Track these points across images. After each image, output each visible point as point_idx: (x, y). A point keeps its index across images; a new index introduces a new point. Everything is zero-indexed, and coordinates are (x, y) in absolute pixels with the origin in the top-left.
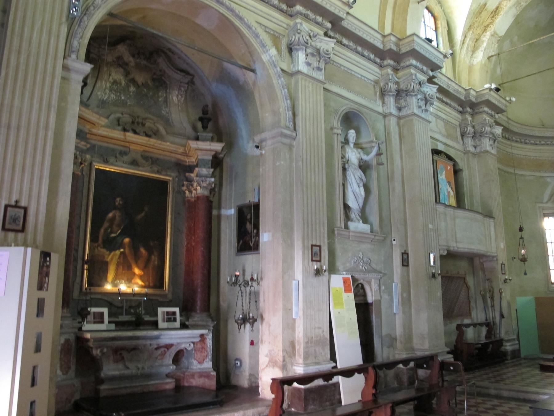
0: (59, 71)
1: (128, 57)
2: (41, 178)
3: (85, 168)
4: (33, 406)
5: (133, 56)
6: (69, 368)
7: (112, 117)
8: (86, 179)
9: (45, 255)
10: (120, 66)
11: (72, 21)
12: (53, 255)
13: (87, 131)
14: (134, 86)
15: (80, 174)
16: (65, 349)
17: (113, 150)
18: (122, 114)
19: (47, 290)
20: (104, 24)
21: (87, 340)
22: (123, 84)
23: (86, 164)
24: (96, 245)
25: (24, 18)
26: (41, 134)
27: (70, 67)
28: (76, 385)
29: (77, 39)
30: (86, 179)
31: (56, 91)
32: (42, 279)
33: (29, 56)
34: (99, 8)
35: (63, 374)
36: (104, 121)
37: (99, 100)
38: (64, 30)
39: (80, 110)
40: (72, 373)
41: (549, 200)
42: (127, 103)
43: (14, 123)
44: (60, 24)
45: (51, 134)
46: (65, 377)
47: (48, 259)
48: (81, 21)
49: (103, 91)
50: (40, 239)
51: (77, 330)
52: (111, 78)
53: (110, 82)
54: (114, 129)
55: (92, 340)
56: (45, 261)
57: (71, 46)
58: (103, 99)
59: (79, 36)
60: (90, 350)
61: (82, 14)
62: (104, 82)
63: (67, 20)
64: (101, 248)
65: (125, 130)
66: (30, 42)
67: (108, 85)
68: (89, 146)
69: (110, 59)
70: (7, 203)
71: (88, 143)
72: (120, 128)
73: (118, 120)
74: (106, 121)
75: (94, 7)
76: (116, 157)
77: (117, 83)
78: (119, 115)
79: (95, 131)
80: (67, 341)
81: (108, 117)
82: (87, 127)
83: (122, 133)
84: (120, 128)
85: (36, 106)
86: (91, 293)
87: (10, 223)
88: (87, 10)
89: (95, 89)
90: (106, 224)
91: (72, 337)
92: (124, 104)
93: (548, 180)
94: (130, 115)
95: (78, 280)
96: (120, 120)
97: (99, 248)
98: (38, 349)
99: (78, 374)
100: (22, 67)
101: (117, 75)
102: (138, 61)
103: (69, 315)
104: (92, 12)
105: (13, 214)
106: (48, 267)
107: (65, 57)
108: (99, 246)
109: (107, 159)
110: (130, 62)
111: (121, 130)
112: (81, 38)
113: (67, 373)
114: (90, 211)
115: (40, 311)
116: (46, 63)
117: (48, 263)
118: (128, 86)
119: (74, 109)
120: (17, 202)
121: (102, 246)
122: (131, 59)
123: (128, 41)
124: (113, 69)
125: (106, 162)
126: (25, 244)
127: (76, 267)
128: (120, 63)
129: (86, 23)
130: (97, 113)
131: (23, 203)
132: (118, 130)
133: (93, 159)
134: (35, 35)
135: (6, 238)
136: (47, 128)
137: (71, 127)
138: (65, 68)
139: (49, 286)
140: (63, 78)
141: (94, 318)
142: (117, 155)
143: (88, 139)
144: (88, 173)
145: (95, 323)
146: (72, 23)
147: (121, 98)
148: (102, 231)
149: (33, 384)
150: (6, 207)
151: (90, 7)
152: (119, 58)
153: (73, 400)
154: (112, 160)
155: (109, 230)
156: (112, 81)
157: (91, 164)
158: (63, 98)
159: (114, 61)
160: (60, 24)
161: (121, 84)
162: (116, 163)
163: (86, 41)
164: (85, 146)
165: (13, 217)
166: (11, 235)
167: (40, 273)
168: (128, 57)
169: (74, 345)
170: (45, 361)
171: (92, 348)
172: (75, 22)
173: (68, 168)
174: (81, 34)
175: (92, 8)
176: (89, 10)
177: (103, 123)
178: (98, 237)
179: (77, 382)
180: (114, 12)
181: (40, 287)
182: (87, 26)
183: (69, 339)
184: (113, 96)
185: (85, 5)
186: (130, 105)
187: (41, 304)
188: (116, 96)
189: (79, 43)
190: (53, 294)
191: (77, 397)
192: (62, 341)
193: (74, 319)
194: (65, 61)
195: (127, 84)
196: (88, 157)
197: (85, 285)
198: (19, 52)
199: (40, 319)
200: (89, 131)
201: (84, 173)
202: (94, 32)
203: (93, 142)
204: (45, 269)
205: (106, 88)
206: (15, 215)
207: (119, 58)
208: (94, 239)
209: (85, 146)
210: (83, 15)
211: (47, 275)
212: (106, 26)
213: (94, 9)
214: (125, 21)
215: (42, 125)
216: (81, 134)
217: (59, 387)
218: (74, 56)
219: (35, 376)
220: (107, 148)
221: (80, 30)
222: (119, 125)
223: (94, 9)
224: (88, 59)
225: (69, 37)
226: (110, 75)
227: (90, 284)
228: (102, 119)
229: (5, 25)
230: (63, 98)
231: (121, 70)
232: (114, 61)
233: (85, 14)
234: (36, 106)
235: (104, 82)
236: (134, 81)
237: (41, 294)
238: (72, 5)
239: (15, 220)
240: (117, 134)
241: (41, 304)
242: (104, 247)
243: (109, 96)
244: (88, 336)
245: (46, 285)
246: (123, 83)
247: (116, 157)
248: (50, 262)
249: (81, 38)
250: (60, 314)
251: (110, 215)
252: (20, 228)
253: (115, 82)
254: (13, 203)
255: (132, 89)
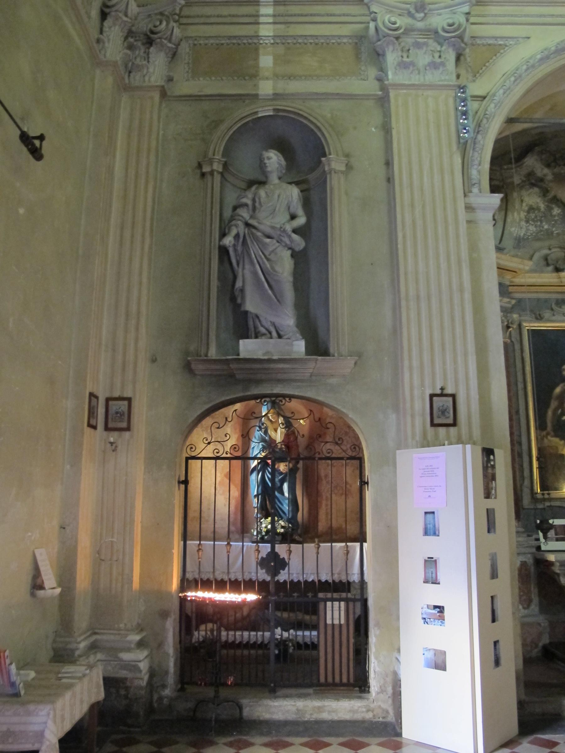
0: (462, 215)
1: (541, 171)
2: (466, 354)
3: (513, 333)
4: (497, 647)
5: (548, 166)
6: (530, 601)
7: (537, 256)
8: (517, 347)
9: (488, 452)
10: (533, 185)
11: (464, 147)
12: (496, 451)
13: (508, 283)
14: (559, 207)
15: (509, 341)
16: (523, 575)
17: (546, 301)
18: (550, 249)
19: (495, 498)
20: (500, 137)
21: (551, 564)
22: (542, 209)
23: (515, 327)
24: (544, 433)
25: (410, 162)
26: (456, 301)
27: (473, 205)
28: (542, 624)
29: (475, 167)
30: (517, 347)
31: (463, 240)
32: (488, 484)
33: (424, 207)
34: (493, 117)
35: (524, 608)
36: (528, 265)
37: (516, 239)
38: (458, 160)
39: (497, 258)
40: (535, 607)
42: (552, 233)
43: (423, 294)
44: (451, 157)
45: (467, 296)
46: (526, 611)
47: (492, 457)
48: (475, 143)
49: (519, 225)
50: (477, 433)
51: (534, 550)
52: (524, 204)
53: (524, 211)
54: (542, 272)
55: (558, 564)
56: (489, 460)
57: (469, 179)
58: (520, 236)
59: (476, 162)
60: (556, 577)
61: (474, 132)
62: (516, 214)
63: (458, 148)
64: (552, 437)
65: (557, 270)
66: (422, 190)
67: (523, 215)
68: (513, 302)
69: (517, 180)
70: (431, 392)
71: (513, 298)
72: (551, 268)
73: (546, 258)
74: (531, 263)
75: (487, 118)
76: (552, 309)
77: (533, 209)
78: (546, 251)
79: (518, 280)
80: (524, 564)
81: (531, 258)
82: (508, 278)
83: (555, 274)
84: (551, 268)
85: (444, 266)
86: (550, 500)
87: (439, 417)
88: (479, 126)
89: (507, 225)
90: (554, 404)
91: (529, 560)
92: (549, 234)
94: (560, 247)
95: (527, 482)
96: (549, 258)
97: (549, 437)
98: (494, 575)
99: (543, 609)
100: (419, 223)
101: (532, 198)
102: (556, 170)
103: (523, 530)
104: (487, 126)
105: (441, 404)
106: (493, 467)
107: (465, 196)
108: (548, 434)
109: (540, 315)
110: (545, 175)
111: (553, 272)
112: (480, 164)
113: (528, 607)
114: (529, 388)
115: (491, 527)
116: (445, 209)
117: (492, 463)
118: (550, 209)
119: (490, 258)
120: (442, 389)
121: (552, 433)
122: (546, 171)
123: (537, 149)
124: (524, 193)
125: (539, 318)
126: (459, 441)
127: (522, 466)
128: (533, 181)
129: (482, 142)
130: (516, 256)
131: (449, 391)
132: (548, 272)
133: (522, 318)
134: (425, 179)
135: (436, 435)
136: (461, 290)
137: (491, 282)
138: (469, 208)
139: (497, 491)
140: (469, 222)
141: (556, 534)
142: (554, 306)
143: (511, 293)
144: (518, 338)
145: (557, 540)
146: (465, 150)
147: (543, 227)
148: (550, 413)
149: (494, 620)
150: (432, 396)
151: (481, 121)
152: (531, 174)
153: (541, 644)
154: (547, 314)
155: (560, 411)
156: (526, 208)
157: (520, 326)
158: (473, 247)
159: (523, 181)
160: (451, 157)
161: (538, 209)
162: (554, 318)
163: (486, 166)
164: (509, 303)
165: (441, 408)
166: (442, 431)
167: (485, 476)
168: (541, 171)
169: (532, 569)
170: (506, 588)
171: (558, 575)
172: (468, 145)
173: (496, 339)
174: (479, 159)
175: (485, 121)
176: (482, 125)
177: (527, 268)
178: (546, 423)
179: (542, 619)
180: (513, 116)
181: (488, 495)
182: (483, 146)
183: (525, 562)
184: (532, 228)
185: (475, 121)
186: (558, 234)
187: (490, 514)
188: (536, 226)
189: (479, 172)
190: (503, 503)
191: (545, 640)
192: (518, 564)
193: (529, 536)
194: (467, 200)
195: (548, 206)
196: (515, 316)
197: (538, 489)
198: (412, 206)
199: (492, 535)
200: (512, 282)
201: (513, 339)
202: (494, 150)
203: (518, 296)
204: (490, 471)
205: (521, 220)
206: (443, 406)
207: (531, 174)
208: (541, 426)
209: (509, 303)
210: (476, 134)
211: (493, 478)
212: (507, 137)
213: (488, 121)
214: (531, 122)
215: (455, 287)
216: (504, 290)
217: (524, 625)
218: (475, 190)
219: (495, 608)
220: (538, 300)
221: (476, 154)
222: (548, 265)
223: (488, 121)
224: (494, 189)
225: (465, 167)
226: (522, 201)
227: (544, 487)
228: (526, 262)
229: (391, 179)
230: (473, 247)
231: (536, 190)
232: (523, 181)
233: (478, 132)
234: (444, 266)
235: (516, 214)
236: (558, 200)
237: (490, 503)
238: (460, 127)
239: (443, 412)
240: (548, 277)
241: (490, 514)
242: (556, 436)
243: (528, 230)
244: (551, 558)
245: (493, 492)
246: (542, 206)
247: (552, 309)
248: (494, 460)
249: (480, 164)
250: (514, 530)
251: (558, 390)
252: (451, 421)
253: (531, 209)
254: (439, 392)
255: (556, 211)
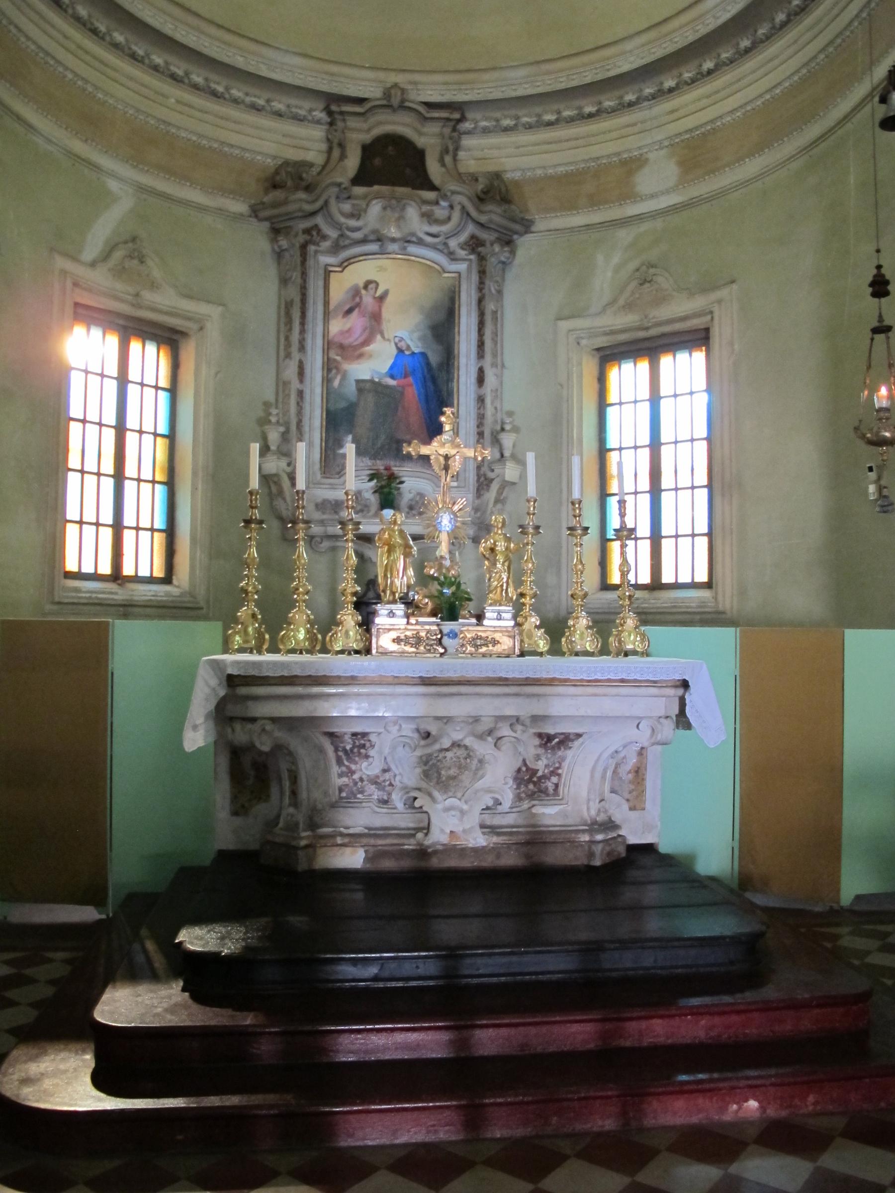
41: (106, 256)
93: (113, 185)
